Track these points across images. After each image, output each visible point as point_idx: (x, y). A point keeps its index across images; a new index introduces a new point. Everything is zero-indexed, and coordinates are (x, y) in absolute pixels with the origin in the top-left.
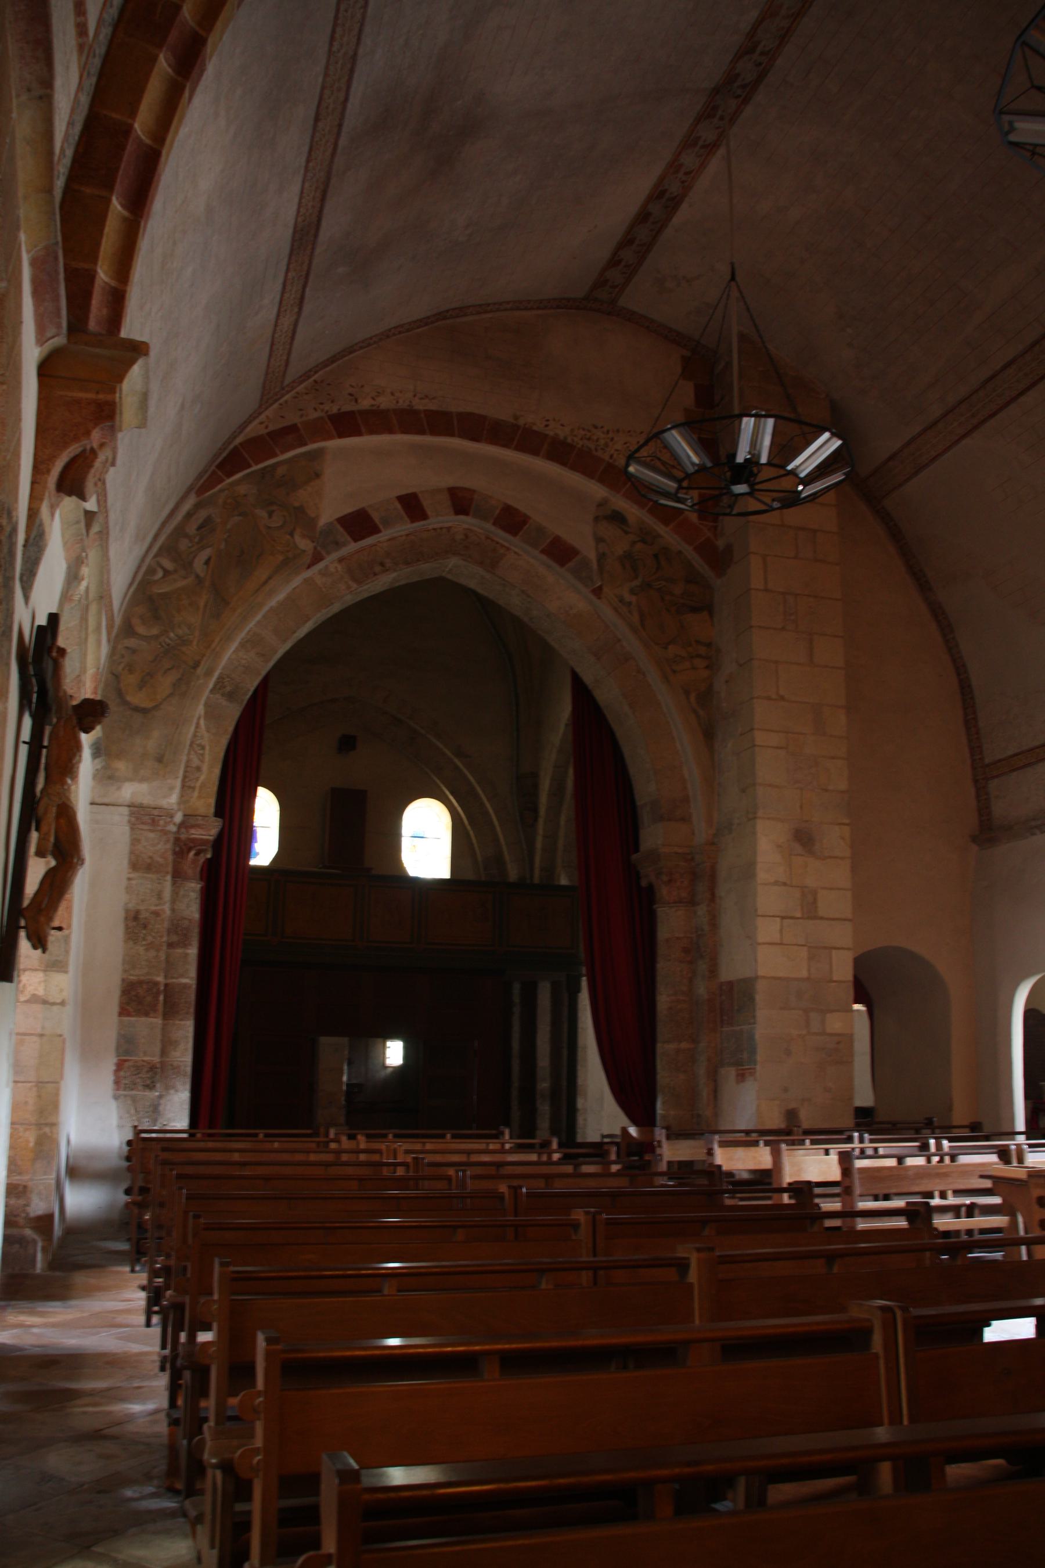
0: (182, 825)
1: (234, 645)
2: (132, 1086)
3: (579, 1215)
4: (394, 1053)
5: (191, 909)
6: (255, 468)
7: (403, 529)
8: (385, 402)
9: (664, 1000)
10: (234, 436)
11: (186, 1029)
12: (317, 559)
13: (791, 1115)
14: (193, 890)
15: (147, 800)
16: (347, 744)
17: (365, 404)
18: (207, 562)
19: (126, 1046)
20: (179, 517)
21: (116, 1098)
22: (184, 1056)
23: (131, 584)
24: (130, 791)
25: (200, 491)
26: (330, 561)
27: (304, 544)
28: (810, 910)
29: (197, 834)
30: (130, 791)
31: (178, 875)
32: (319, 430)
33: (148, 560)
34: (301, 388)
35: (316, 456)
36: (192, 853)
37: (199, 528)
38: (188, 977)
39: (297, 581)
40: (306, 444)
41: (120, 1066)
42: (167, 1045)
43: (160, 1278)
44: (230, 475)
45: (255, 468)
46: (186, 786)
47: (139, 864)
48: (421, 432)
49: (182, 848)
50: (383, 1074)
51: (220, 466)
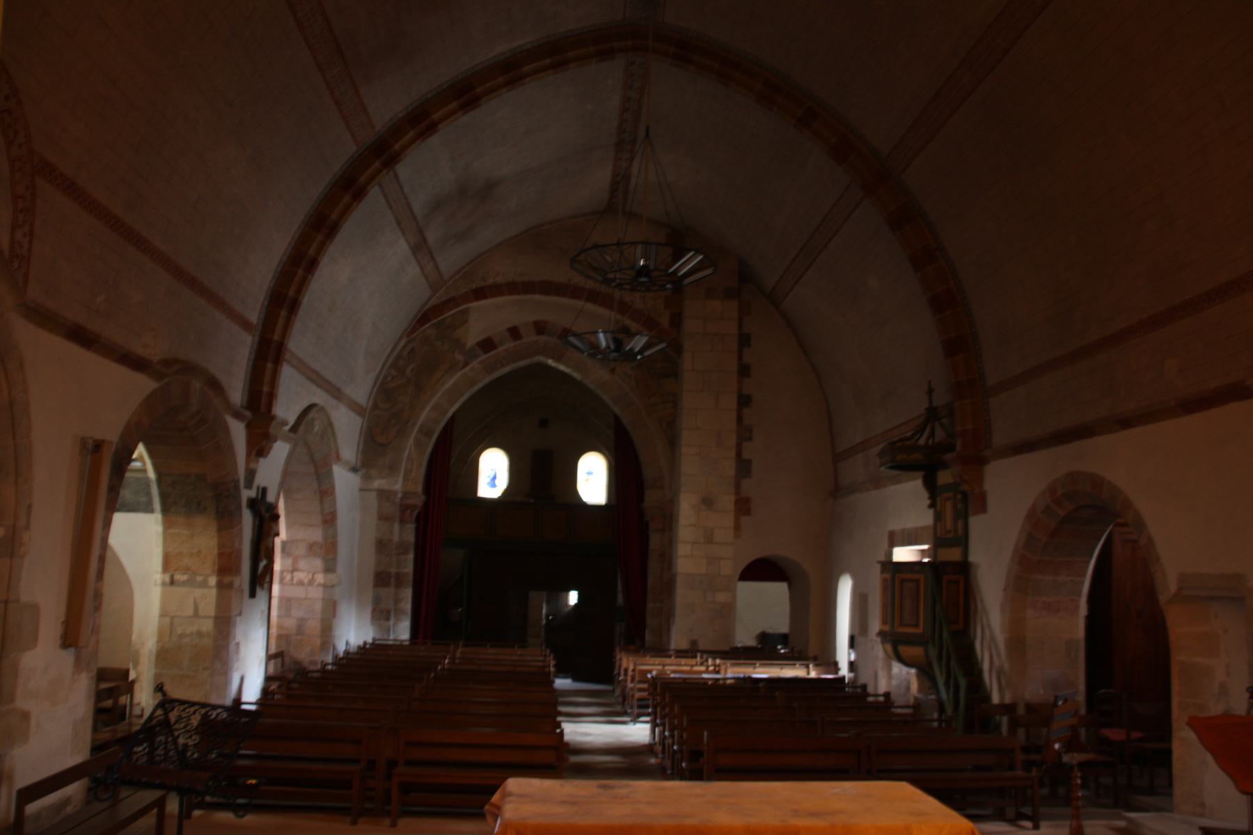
0: (402, 499)
1: (428, 408)
2: (379, 619)
3: (777, 694)
4: (573, 597)
5: (410, 536)
6: (434, 321)
7: (511, 344)
8: (500, 280)
9: (650, 580)
10: (426, 303)
11: (408, 593)
12: (466, 364)
13: (694, 643)
14: (411, 529)
15: (385, 487)
16: (544, 423)
17: (490, 281)
18: (412, 370)
19: (377, 601)
20: (399, 348)
21: (372, 624)
22: (407, 606)
23: (373, 387)
24: (378, 483)
25: (410, 334)
26: (475, 364)
27: (459, 357)
28: (709, 538)
29: (411, 502)
30: (378, 483)
31: (403, 522)
32: (466, 298)
33: (384, 371)
34: (457, 277)
35: (466, 311)
36: (409, 511)
37: (409, 353)
38: (409, 568)
39: (458, 375)
40: (459, 306)
41: (374, 611)
42: (397, 601)
43: (703, 735)
44: (423, 325)
45: (434, 321)
46: (406, 479)
47: (383, 517)
48: (519, 293)
49: (404, 508)
50: (567, 610)
51: (419, 321)
